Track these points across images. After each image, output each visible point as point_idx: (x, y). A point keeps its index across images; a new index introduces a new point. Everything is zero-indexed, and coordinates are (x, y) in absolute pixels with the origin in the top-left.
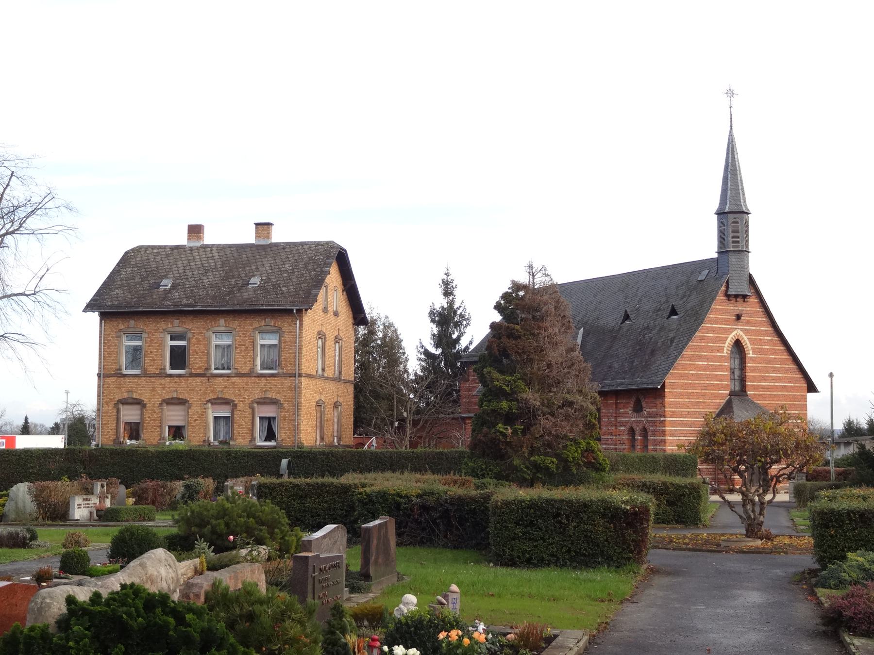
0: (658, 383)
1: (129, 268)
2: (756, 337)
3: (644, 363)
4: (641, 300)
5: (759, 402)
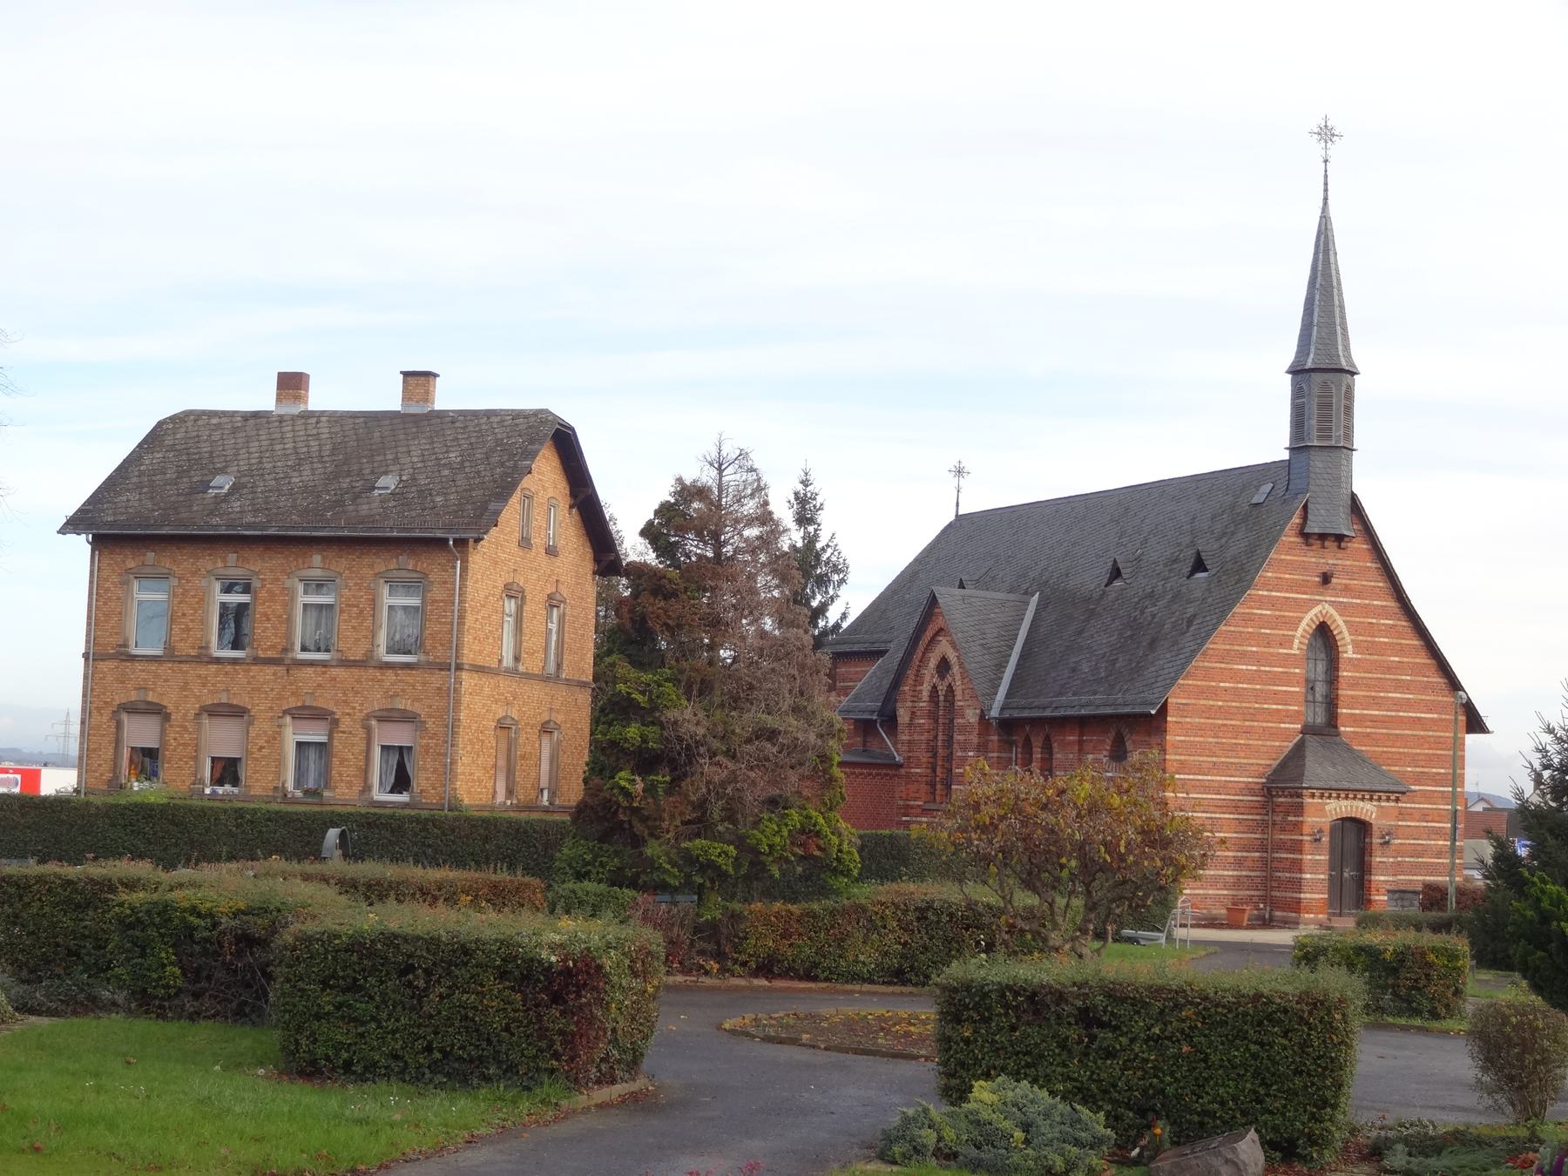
0: (1153, 704)
1: (158, 452)
2: (1362, 620)
3: (1134, 665)
4: (1146, 540)
5: (1363, 748)
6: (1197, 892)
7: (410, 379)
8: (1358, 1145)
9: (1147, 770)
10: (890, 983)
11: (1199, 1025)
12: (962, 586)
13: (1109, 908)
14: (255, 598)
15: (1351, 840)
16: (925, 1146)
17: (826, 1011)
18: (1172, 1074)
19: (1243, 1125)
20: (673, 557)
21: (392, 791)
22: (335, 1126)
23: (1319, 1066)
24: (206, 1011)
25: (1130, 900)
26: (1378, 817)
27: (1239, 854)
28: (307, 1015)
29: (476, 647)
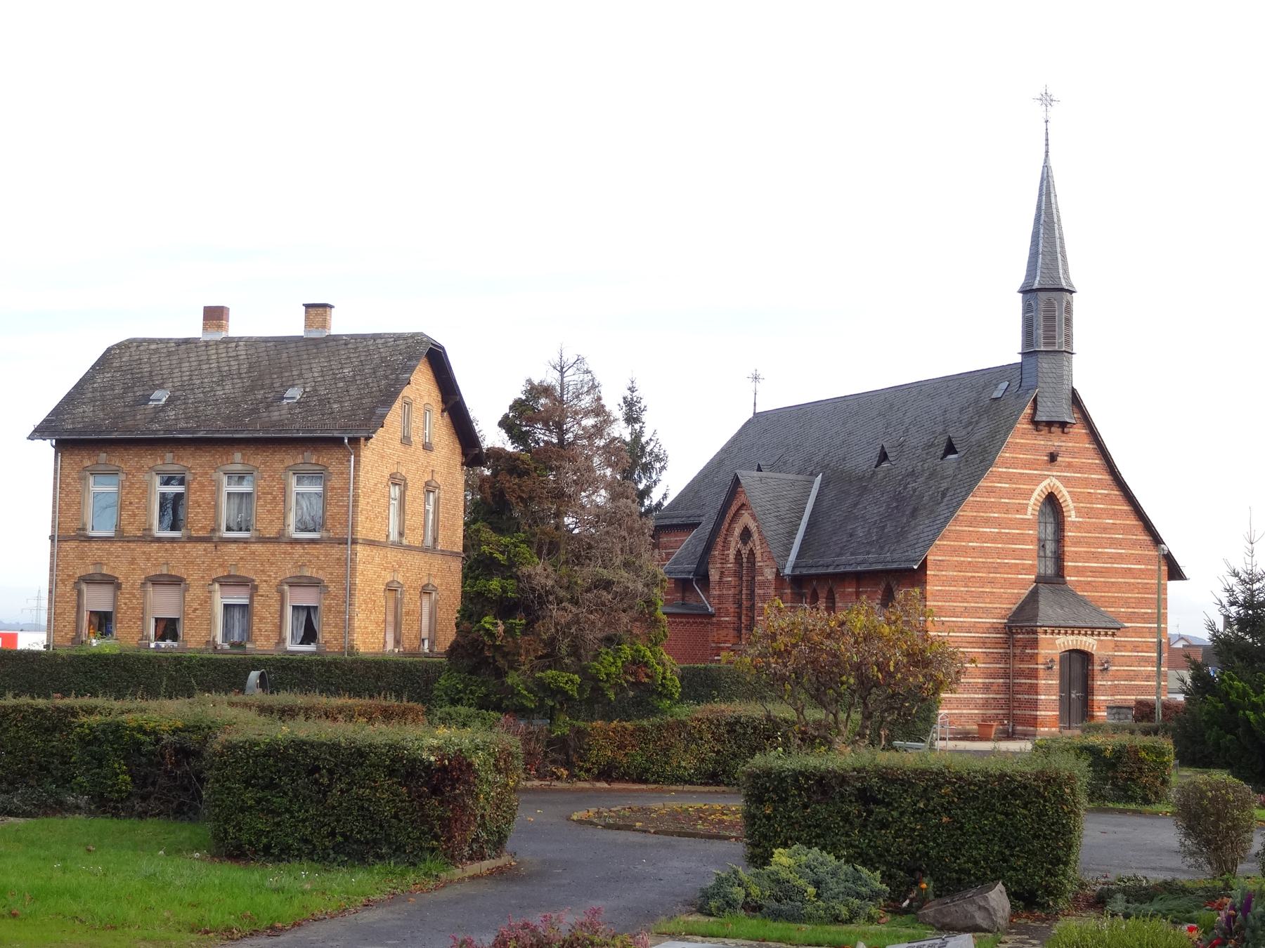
0: (915, 561)
1: (108, 373)
2: (1082, 490)
4: (907, 430)
5: (1086, 594)
6: (953, 711)
7: (312, 311)
8: (1085, 896)
9: (911, 605)
10: (706, 784)
11: (956, 800)
12: (759, 469)
13: (883, 717)
14: (188, 489)
15: (1077, 668)
16: (735, 900)
17: (656, 805)
18: (934, 840)
19: (993, 880)
20: (525, 444)
21: (301, 643)
22: (257, 895)
23: (1053, 831)
24: (152, 810)
25: (899, 709)
26: (1098, 649)
27: (987, 681)
28: (234, 809)
29: (368, 525)
